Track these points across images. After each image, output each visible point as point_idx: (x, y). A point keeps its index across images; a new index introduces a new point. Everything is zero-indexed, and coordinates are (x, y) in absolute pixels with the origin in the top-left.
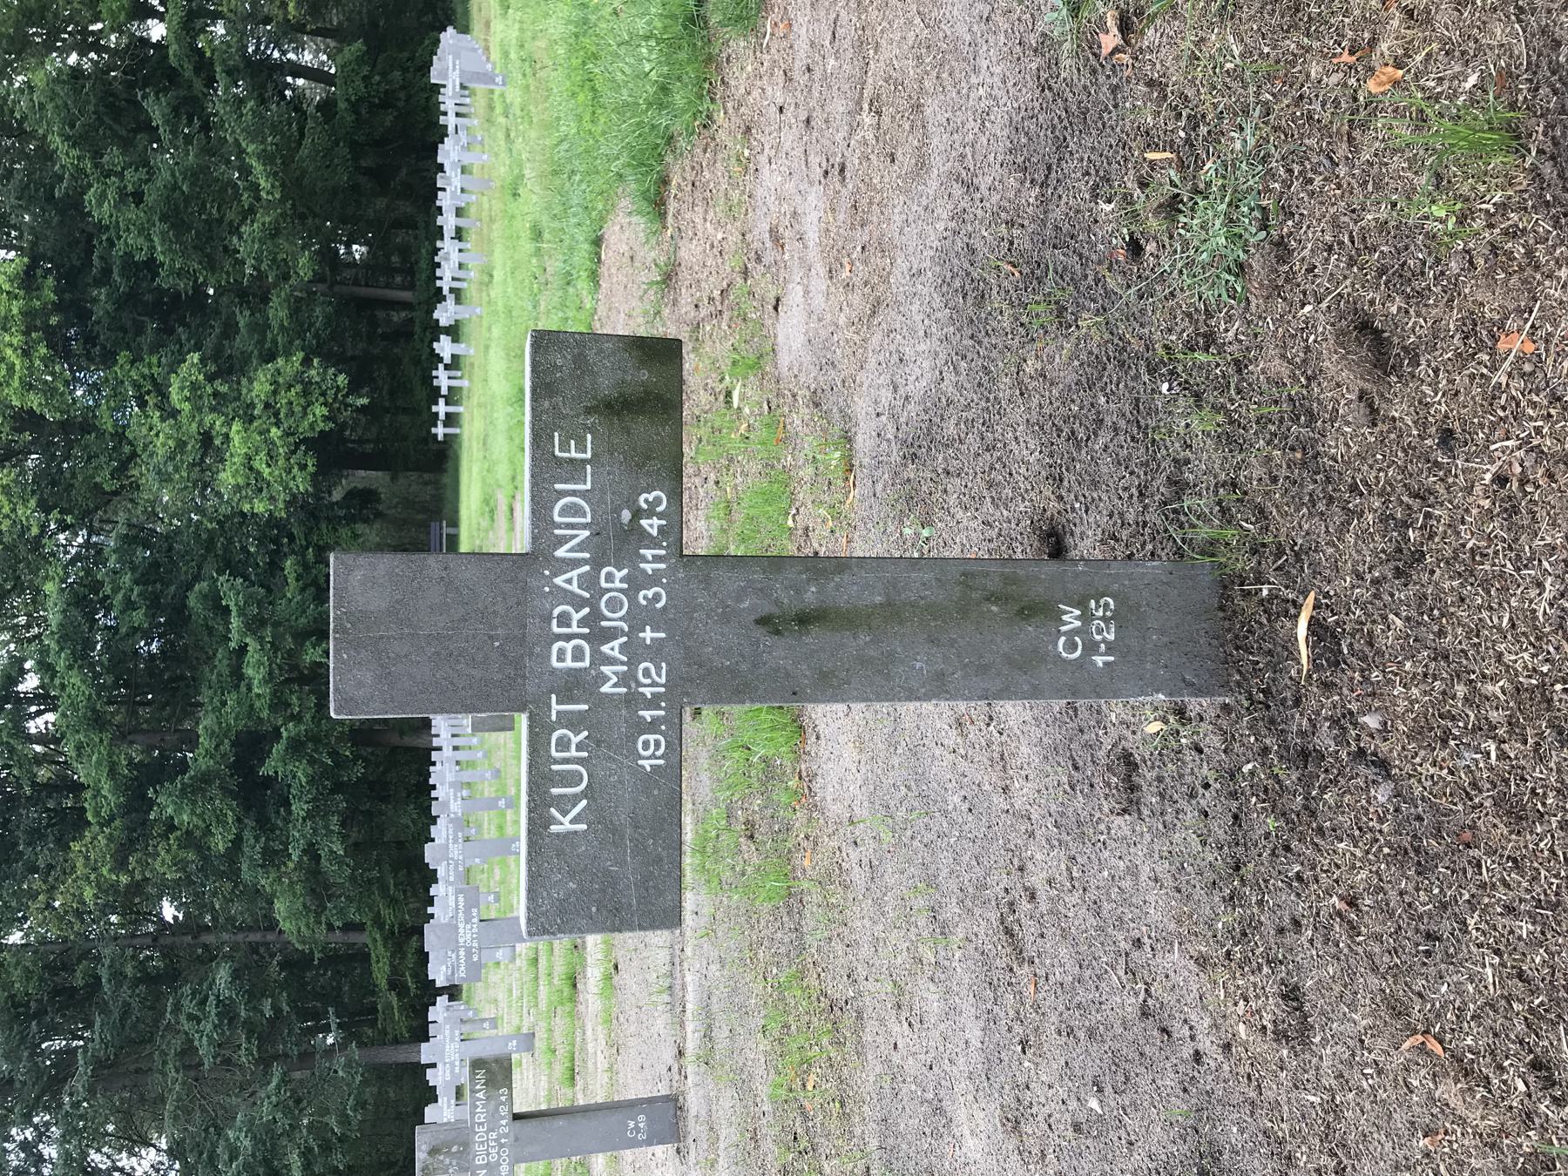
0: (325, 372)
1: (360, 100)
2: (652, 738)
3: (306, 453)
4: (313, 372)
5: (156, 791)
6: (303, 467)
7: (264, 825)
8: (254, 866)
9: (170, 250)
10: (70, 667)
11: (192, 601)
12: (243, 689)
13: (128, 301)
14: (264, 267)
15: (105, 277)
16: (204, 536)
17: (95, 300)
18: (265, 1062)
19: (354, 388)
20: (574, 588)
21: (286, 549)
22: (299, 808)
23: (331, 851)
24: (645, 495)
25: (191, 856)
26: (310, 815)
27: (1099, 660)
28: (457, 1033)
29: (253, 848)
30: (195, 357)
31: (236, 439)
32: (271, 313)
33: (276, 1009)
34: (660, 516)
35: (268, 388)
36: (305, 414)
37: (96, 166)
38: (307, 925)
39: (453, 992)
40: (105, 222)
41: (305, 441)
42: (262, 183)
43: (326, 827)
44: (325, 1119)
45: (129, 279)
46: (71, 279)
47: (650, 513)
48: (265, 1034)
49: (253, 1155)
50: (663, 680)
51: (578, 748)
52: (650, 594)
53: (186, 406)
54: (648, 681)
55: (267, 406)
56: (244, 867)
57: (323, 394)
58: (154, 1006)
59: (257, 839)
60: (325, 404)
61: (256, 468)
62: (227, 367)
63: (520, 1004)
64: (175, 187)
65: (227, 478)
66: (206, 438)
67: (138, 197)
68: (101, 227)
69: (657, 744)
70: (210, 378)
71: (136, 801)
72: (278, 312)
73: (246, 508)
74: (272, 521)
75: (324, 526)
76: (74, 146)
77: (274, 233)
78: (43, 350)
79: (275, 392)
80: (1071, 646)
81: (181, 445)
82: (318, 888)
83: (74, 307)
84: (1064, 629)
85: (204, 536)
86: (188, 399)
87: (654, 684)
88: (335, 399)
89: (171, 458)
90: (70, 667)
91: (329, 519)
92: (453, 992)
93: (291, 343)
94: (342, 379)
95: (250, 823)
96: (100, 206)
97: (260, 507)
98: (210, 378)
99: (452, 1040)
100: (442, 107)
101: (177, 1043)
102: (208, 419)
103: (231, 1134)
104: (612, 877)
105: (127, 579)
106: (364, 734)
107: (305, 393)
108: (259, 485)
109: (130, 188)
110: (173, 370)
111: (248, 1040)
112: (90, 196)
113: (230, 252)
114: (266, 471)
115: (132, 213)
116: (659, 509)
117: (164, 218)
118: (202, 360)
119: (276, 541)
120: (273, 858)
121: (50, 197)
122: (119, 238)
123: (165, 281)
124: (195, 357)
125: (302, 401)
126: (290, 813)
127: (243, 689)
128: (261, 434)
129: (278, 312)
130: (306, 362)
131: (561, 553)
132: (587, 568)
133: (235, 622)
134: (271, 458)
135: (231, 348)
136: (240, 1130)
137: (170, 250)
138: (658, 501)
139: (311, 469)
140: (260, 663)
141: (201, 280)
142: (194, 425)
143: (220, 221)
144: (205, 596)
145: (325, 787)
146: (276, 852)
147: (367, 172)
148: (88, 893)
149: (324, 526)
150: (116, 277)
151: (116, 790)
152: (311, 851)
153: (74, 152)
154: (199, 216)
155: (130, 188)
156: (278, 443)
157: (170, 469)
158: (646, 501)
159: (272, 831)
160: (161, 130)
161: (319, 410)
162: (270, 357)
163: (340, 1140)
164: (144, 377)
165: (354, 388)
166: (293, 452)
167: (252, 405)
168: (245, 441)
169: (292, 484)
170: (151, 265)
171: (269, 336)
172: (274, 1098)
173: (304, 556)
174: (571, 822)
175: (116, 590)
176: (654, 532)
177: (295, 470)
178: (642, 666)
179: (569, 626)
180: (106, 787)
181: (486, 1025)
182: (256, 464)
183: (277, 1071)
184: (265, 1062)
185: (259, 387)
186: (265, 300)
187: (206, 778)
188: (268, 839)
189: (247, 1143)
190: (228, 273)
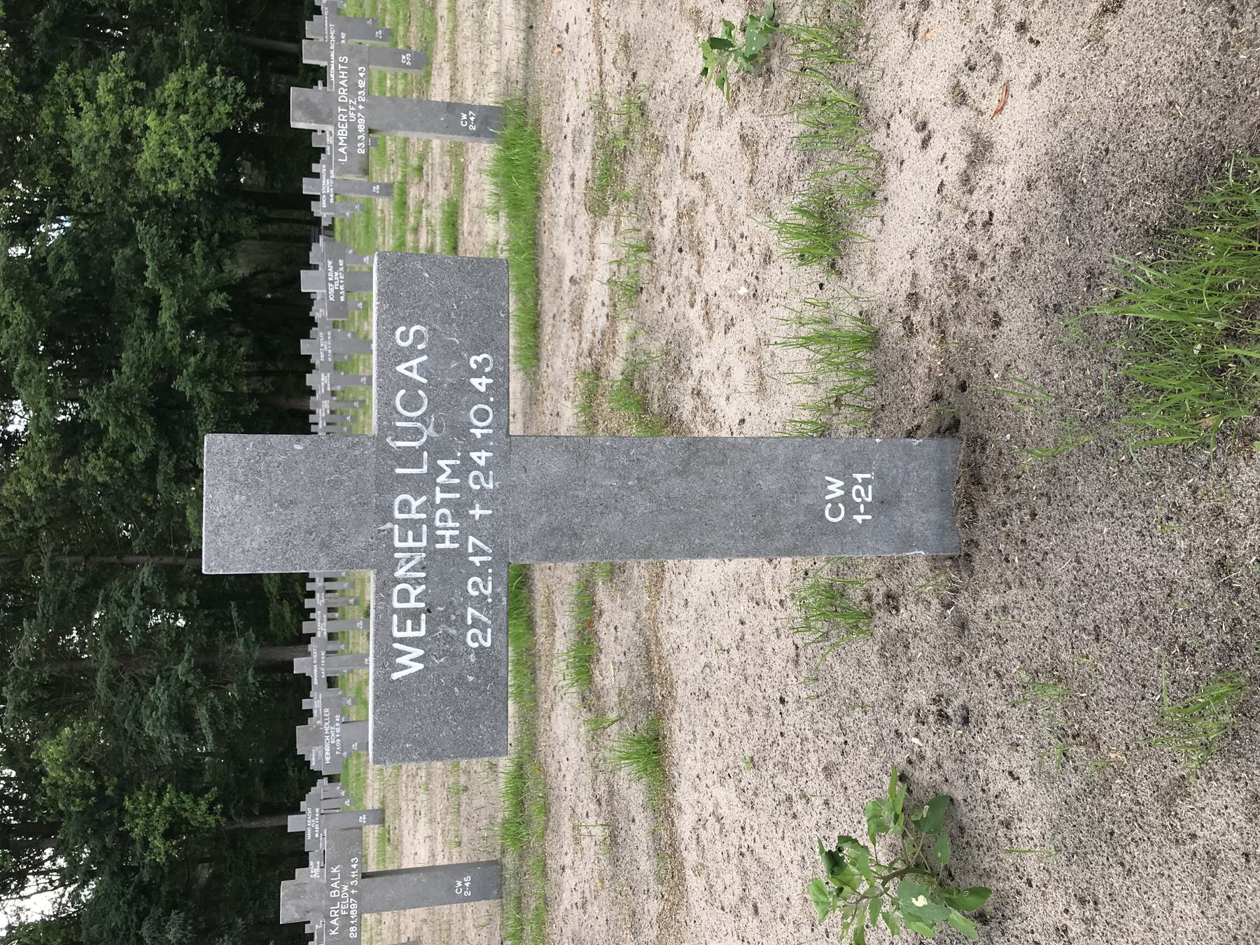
4: (216, 79)
6: (210, 156)
17: (36, 23)
19: (251, 95)
20: (414, 375)
21: (195, 235)
24: (474, 358)
27: (859, 518)
34: (488, 375)
36: (211, 112)
47: (478, 373)
51: (418, 599)
52: (480, 359)
56: (160, 479)
57: (225, 98)
59: (170, 456)
65: (146, 159)
66: (126, 136)
75: (226, 216)
80: (835, 513)
84: (828, 497)
88: (235, 102)
93: (197, 58)
94: (240, 86)
97: (173, 186)
106: (248, 589)
130: (212, 73)
131: (400, 573)
132: (425, 358)
134: (183, 139)
139: (217, 158)
142: (116, 118)
146: (187, 471)
158: (476, 362)
159: (183, 452)
165: (251, 95)
167: (164, 106)
176: (483, 389)
177: (203, 157)
178: (470, 582)
179: (408, 601)
185: (172, 84)
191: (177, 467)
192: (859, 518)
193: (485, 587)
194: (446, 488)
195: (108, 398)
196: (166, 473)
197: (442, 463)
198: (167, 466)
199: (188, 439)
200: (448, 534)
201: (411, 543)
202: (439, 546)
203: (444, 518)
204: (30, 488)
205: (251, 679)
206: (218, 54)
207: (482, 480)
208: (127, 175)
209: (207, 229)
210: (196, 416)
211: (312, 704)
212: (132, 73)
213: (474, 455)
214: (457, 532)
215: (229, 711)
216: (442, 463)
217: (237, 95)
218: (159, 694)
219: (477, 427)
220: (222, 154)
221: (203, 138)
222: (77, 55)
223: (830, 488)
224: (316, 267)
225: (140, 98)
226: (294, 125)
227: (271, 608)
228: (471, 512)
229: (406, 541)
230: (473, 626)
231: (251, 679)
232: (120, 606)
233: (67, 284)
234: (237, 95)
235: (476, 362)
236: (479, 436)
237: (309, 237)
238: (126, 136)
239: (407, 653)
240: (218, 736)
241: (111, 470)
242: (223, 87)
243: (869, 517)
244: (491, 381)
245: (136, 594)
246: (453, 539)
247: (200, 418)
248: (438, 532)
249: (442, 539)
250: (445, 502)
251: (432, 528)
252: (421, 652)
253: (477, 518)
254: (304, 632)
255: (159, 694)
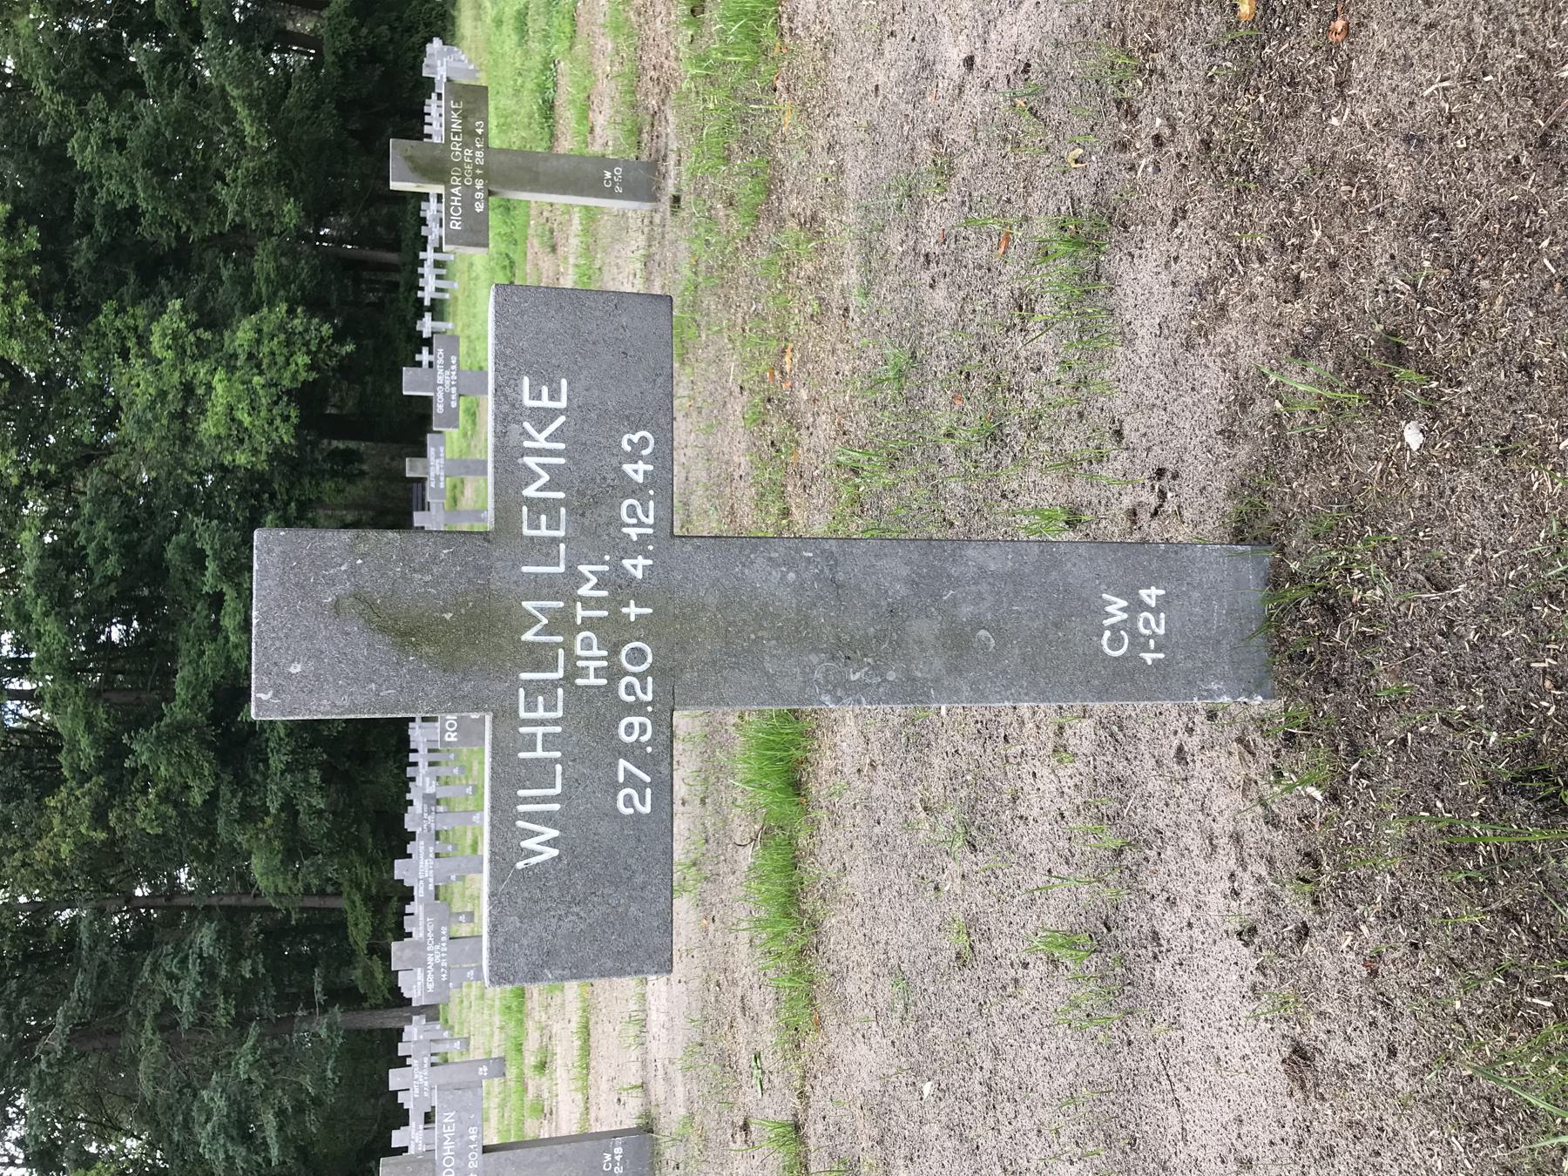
0: (309, 322)
1: (346, 54)
2: (636, 720)
3: (288, 404)
4: (296, 321)
5: (130, 737)
6: (286, 419)
7: (241, 781)
8: (231, 821)
9: (153, 196)
10: (46, 614)
11: (171, 553)
12: (221, 641)
13: (108, 253)
14: (247, 214)
15: (87, 227)
16: (184, 491)
17: (77, 251)
18: (240, 1023)
22: (277, 762)
23: (310, 805)
25: (171, 812)
26: (289, 768)
28: (431, 849)
29: (230, 804)
30: (178, 304)
31: (219, 388)
32: (256, 266)
33: (254, 971)
35: (252, 335)
37: (80, 113)
38: (285, 881)
39: (431, 1012)
40: (88, 168)
41: (289, 392)
42: (248, 129)
43: (306, 781)
44: (300, 1079)
45: (111, 229)
46: (55, 234)
47: (634, 457)
48: (244, 994)
49: (228, 1116)
50: (651, 521)
52: (636, 438)
53: (170, 354)
54: (634, 521)
55: (250, 356)
56: (221, 822)
57: (307, 344)
58: (132, 968)
59: (234, 796)
60: (309, 353)
61: (239, 409)
62: (212, 319)
63: (502, 1058)
64: (158, 134)
65: (208, 427)
66: (188, 389)
67: (121, 143)
68: (84, 177)
69: (643, 730)
70: (193, 327)
71: (113, 754)
72: (263, 264)
73: (227, 459)
74: (253, 475)
75: (306, 481)
76: (58, 90)
77: (256, 181)
78: (24, 298)
79: (258, 342)
80: (1116, 642)
81: (162, 394)
82: (295, 849)
83: (53, 254)
84: (1107, 622)
85: (184, 491)
86: (169, 347)
87: (640, 524)
89: (152, 407)
90: (46, 614)
91: (312, 475)
92: (431, 1012)
93: (275, 294)
95: (227, 777)
96: (83, 152)
97: (242, 458)
98: (193, 327)
99: (426, 856)
100: (427, 119)
101: (155, 1005)
102: (190, 369)
103: (204, 1093)
104: (595, 911)
105: (101, 525)
107: (288, 343)
108: (241, 436)
109: (113, 134)
110: (154, 317)
111: (226, 1002)
112: (73, 143)
113: (212, 200)
114: (247, 420)
115: (116, 160)
116: (645, 452)
117: (147, 164)
118: (183, 307)
119: (257, 496)
120: (250, 815)
121: (33, 147)
122: (102, 186)
123: (146, 229)
124: (178, 304)
125: (285, 351)
126: (268, 767)
127: (221, 641)
128: (243, 383)
129: (263, 264)
130: (291, 311)
133: (211, 566)
134: (253, 409)
135: (215, 300)
136: (215, 1091)
137: (153, 196)
138: (644, 442)
139: (295, 420)
140: (236, 610)
141: (184, 229)
142: (177, 374)
143: (206, 169)
144: (183, 549)
145: (303, 740)
147: (353, 134)
148: (65, 850)
149: (306, 481)
150: (98, 227)
151: (95, 743)
152: (289, 806)
153: (59, 98)
154: (180, 162)
155: (113, 134)
156: (261, 392)
157: (149, 416)
158: (630, 442)
160: (146, 76)
161: (302, 359)
162: (254, 309)
163: (313, 1100)
164: (128, 328)
165: (339, 337)
166: (276, 403)
167: (235, 356)
168: (228, 390)
169: (274, 435)
170: (133, 214)
171: (255, 288)
172: (250, 1058)
173: (285, 510)
174: (546, 439)
175: (89, 540)
176: (640, 478)
177: (278, 422)
180: (84, 742)
181: (462, 918)
182: (239, 415)
183: (254, 1030)
184: (240, 1023)
185: (242, 335)
186: (251, 251)
187: (182, 728)
188: (245, 795)
189: (222, 1103)
190: (212, 224)
191: (243, 806)
192: (1148, 658)
193: (643, 802)
194: (587, 603)
195: (158, 738)
196: (228, 814)
197: (584, 569)
198: (230, 804)
199: (256, 768)
200: (593, 664)
201: (541, 713)
202: (579, 682)
203: (587, 645)
204: (65, 850)
205: (329, 1074)
206: (302, 288)
207: (639, 511)
208: (186, 440)
209: (282, 496)
210: (267, 740)
211: (426, 468)
212: (193, 317)
213: (627, 563)
214: (605, 664)
215: (300, 1109)
216: (584, 569)
217: (322, 340)
218: (214, 1098)
219: (628, 525)
220: (300, 417)
221: (280, 398)
222: (127, 291)
223: (1109, 609)
224: (410, 856)
225: (203, 351)
226: (395, 185)
227: (364, 767)
228: (625, 610)
229: (538, 527)
230: (625, 785)
231: (329, 1074)
232: (171, 976)
233: (110, 579)
234: (322, 340)
235: (630, 442)
236: (635, 538)
237: (409, 501)
238: (188, 389)
239: (538, 834)
240: (285, 1142)
241: (162, 819)
242: (307, 330)
243: (1161, 656)
244: (650, 468)
245: (194, 968)
246: (598, 673)
247: (271, 744)
248: (580, 663)
249: (583, 672)
250: (589, 624)
251: (571, 657)
252: (555, 833)
253: (632, 619)
254: (400, 1054)
255: (214, 1098)
